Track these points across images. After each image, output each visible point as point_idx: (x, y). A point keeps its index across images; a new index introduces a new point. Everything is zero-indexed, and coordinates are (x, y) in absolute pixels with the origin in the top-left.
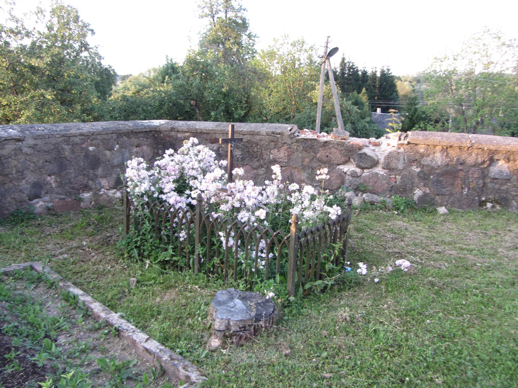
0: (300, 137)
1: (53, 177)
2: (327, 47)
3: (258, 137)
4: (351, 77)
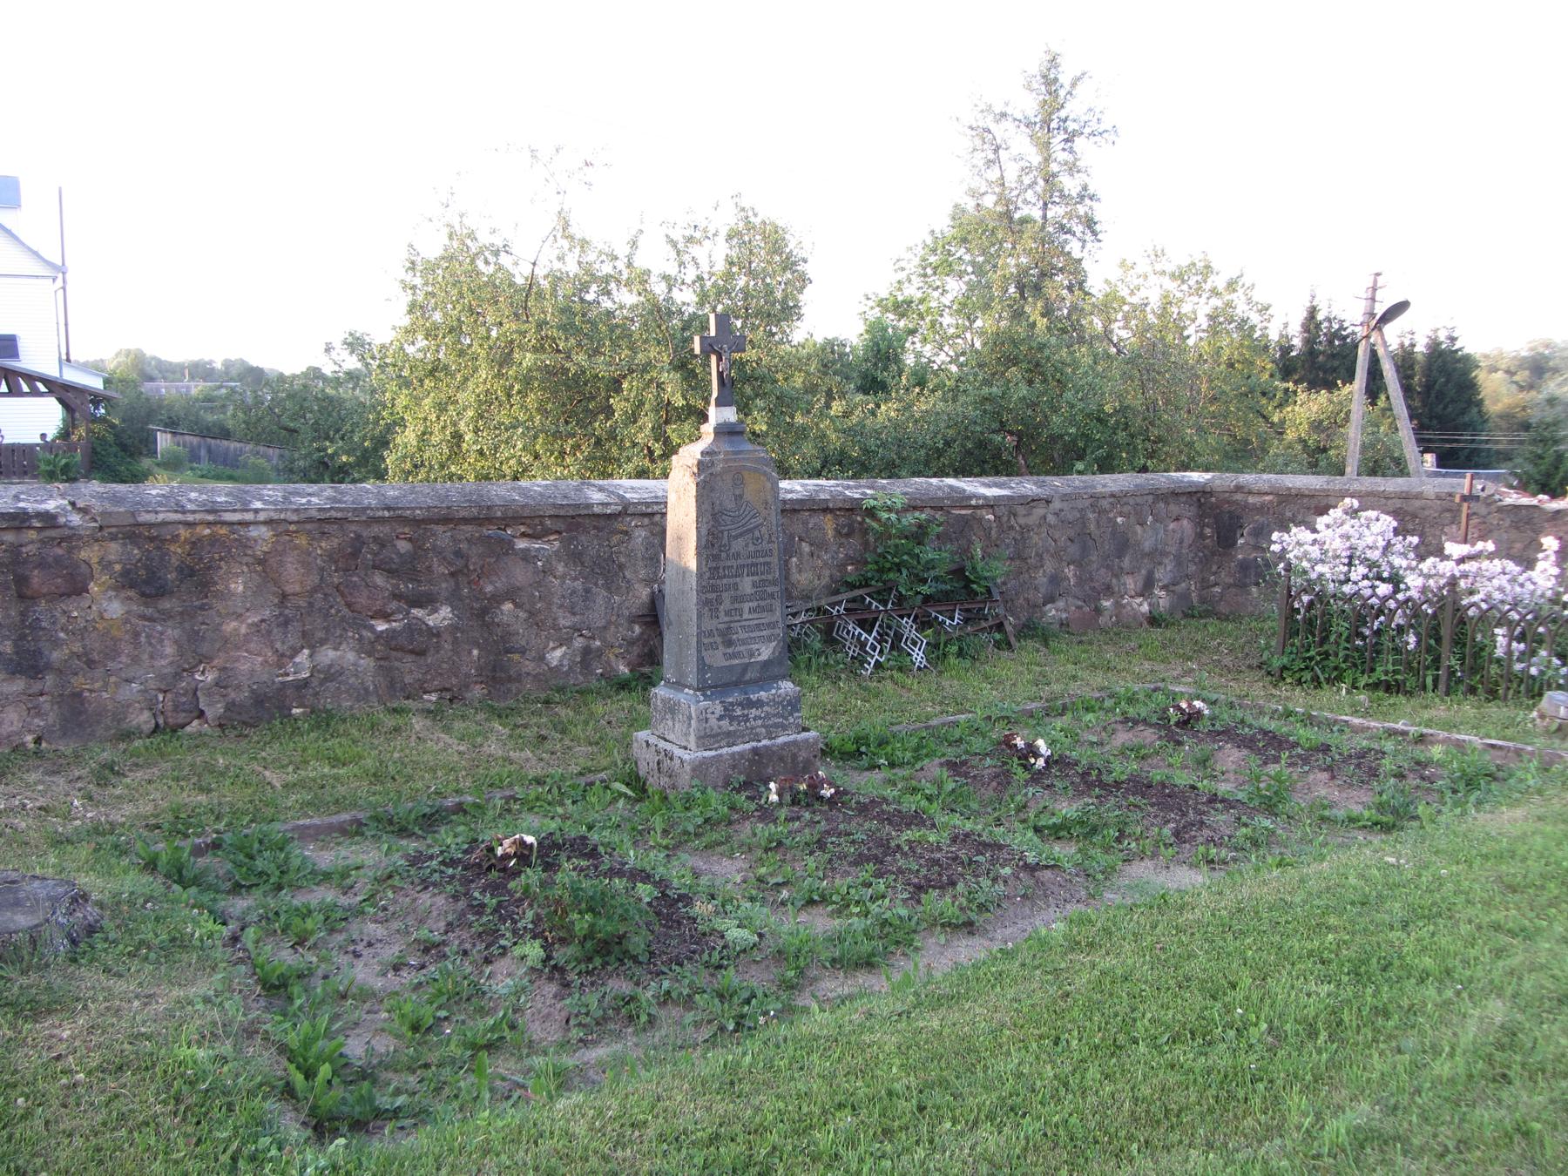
0: (1504, 503)
1: (1072, 567)
2: (1373, 299)
3: (1418, 503)
4: (1336, 363)
